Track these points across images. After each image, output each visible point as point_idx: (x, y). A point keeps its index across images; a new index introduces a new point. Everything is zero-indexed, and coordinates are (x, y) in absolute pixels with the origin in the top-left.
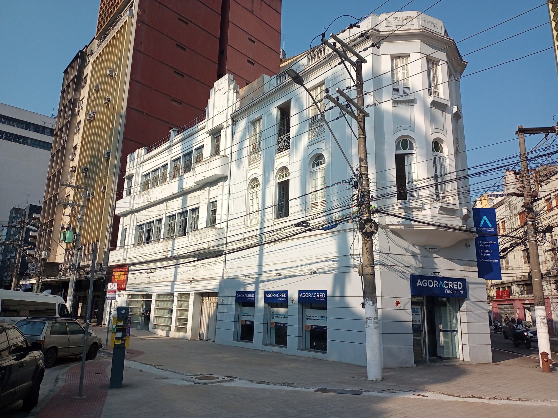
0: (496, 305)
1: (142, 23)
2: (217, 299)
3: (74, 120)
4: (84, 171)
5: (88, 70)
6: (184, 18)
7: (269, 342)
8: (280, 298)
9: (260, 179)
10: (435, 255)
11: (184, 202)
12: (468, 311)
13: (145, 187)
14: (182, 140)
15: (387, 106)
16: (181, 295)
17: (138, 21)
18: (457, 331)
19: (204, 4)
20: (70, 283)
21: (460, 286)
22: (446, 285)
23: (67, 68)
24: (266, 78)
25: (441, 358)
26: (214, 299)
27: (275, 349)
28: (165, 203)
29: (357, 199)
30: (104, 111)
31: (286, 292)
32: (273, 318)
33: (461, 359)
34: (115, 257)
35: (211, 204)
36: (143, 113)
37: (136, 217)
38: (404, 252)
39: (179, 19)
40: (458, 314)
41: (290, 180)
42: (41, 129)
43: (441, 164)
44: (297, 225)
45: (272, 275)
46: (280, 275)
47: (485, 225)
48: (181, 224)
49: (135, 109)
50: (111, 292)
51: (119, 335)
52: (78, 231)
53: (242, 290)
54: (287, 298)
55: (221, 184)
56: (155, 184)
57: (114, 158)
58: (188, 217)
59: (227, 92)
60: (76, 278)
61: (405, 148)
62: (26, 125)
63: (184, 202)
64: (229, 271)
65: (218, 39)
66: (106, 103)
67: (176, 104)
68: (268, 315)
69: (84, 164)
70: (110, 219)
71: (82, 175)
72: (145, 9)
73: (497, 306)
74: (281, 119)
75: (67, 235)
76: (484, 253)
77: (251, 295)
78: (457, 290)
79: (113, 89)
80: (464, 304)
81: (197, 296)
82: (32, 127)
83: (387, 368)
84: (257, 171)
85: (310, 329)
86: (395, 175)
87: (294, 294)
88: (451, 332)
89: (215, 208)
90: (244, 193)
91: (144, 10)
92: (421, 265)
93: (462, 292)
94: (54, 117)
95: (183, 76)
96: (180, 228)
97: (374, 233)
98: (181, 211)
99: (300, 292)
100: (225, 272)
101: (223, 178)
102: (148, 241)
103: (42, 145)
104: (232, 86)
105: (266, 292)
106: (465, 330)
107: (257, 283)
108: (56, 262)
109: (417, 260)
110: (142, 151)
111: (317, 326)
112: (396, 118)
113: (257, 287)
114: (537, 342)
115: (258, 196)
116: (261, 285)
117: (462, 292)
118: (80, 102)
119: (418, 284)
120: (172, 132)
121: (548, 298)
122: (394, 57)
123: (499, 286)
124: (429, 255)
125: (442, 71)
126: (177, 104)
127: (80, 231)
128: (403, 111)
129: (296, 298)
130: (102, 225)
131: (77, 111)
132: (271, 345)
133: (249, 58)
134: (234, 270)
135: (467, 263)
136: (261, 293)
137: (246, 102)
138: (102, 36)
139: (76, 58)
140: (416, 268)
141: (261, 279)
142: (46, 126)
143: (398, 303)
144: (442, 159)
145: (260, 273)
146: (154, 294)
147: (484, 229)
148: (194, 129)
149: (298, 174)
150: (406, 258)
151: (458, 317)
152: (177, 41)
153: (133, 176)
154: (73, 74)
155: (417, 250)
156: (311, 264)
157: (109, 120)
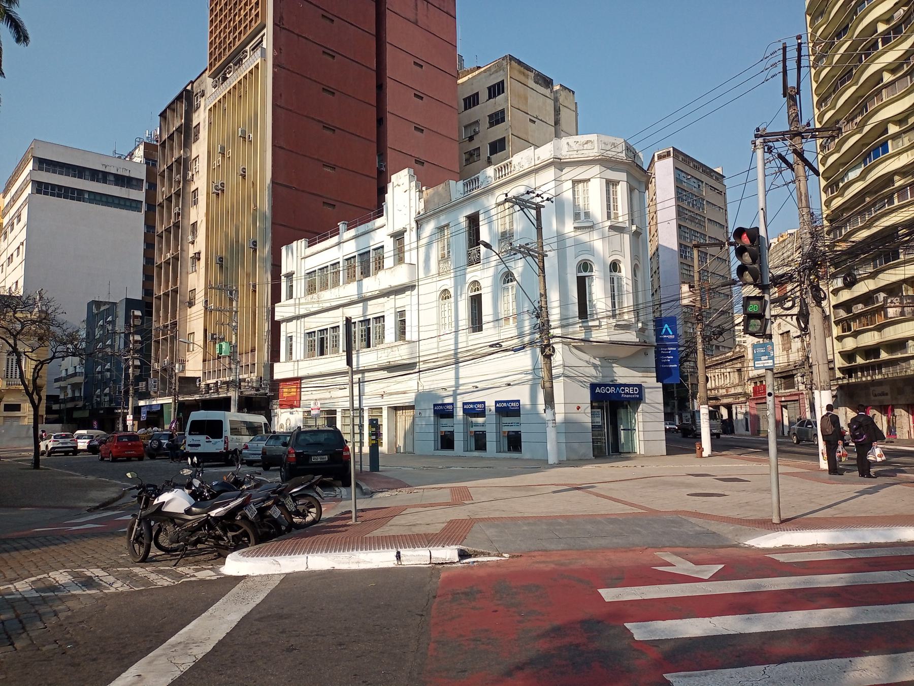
0: (753, 404)
1: (279, 68)
2: (412, 413)
3: (188, 188)
4: (218, 261)
5: (201, 117)
6: (329, 49)
7: (469, 449)
8: (478, 408)
9: (452, 291)
10: (614, 365)
11: (365, 309)
12: (644, 412)
13: (311, 289)
14: (356, 237)
15: (569, 227)
16: (371, 409)
17: (274, 66)
18: (635, 430)
19: (352, 25)
20: (232, 402)
21: (636, 390)
22: (623, 390)
23: (165, 111)
24: (452, 182)
25: (621, 453)
26: (410, 413)
27: (476, 454)
28: (341, 309)
29: (539, 328)
30: (238, 184)
31: (484, 403)
32: (472, 427)
33: (638, 453)
34: (281, 371)
35: (398, 314)
36: (291, 188)
37: (302, 323)
38: (586, 364)
39: (324, 52)
40: (636, 415)
41: (482, 296)
42: (100, 176)
43: (618, 283)
44: (491, 346)
45: (469, 387)
46: (477, 387)
47: (667, 333)
48: (363, 334)
49: (281, 185)
50: (315, 409)
51: (374, 437)
52: (234, 342)
53: (440, 402)
54: (484, 408)
55: (408, 293)
56: (324, 287)
57: (264, 246)
58: (371, 326)
59: (408, 191)
60: (239, 396)
61: (585, 271)
62: (79, 172)
63: (365, 309)
64: (425, 384)
65: (374, 70)
66: (242, 175)
67: (328, 170)
68: (467, 424)
69: (217, 253)
70: (266, 325)
71: (215, 267)
72: (282, 47)
73: (754, 405)
74: (470, 227)
75: (224, 347)
76: (664, 359)
77: (448, 407)
78: (634, 394)
79: (249, 157)
80: (641, 407)
81: (390, 409)
82: (87, 173)
83: (569, 460)
84: (448, 283)
85: (506, 435)
86: (577, 297)
87: (490, 404)
88: (630, 430)
89: (403, 318)
90: (435, 304)
91: (280, 49)
92: (601, 375)
93: (638, 396)
94: (117, 156)
95: (334, 130)
96: (362, 337)
97: (551, 355)
98: (362, 319)
99: (496, 402)
100: (419, 385)
101: (410, 287)
102: (322, 353)
103: (111, 201)
104: (413, 184)
105: (464, 404)
106: (641, 429)
107: (455, 395)
108: (187, 376)
109: (837, 275)
110: (302, 243)
111: (513, 432)
112: (578, 243)
113: (455, 399)
114: (701, 438)
115: (450, 308)
116: (458, 397)
117: (638, 396)
118: (193, 162)
119: (597, 391)
120: (341, 226)
121: (802, 394)
122: (575, 182)
123: (757, 380)
124: (609, 365)
125: (621, 190)
126: (329, 170)
127: (236, 342)
128: (585, 237)
129: (493, 408)
130: (257, 332)
131: (190, 175)
132: (471, 451)
133: (417, 90)
134: (430, 383)
135: (646, 370)
136: (459, 405)
137: (431, 207)
138: (220, 75)
139: (179, 98)
140: (596, 377)
141: (459, 392)
142: (107, 170)
143: (578, 408)
144: (620, 278)
145: (457, 386)
146: (338, 410)
147: (665, 336)
148: (370, 225)
149: (489, 289)
150: (587, 370)
151: (636, 418)
152: (323, 84)
153: (294, 273)
154: (178, 122)
155: (597, 362)
156: (505, 377)
157: (249, 197)
